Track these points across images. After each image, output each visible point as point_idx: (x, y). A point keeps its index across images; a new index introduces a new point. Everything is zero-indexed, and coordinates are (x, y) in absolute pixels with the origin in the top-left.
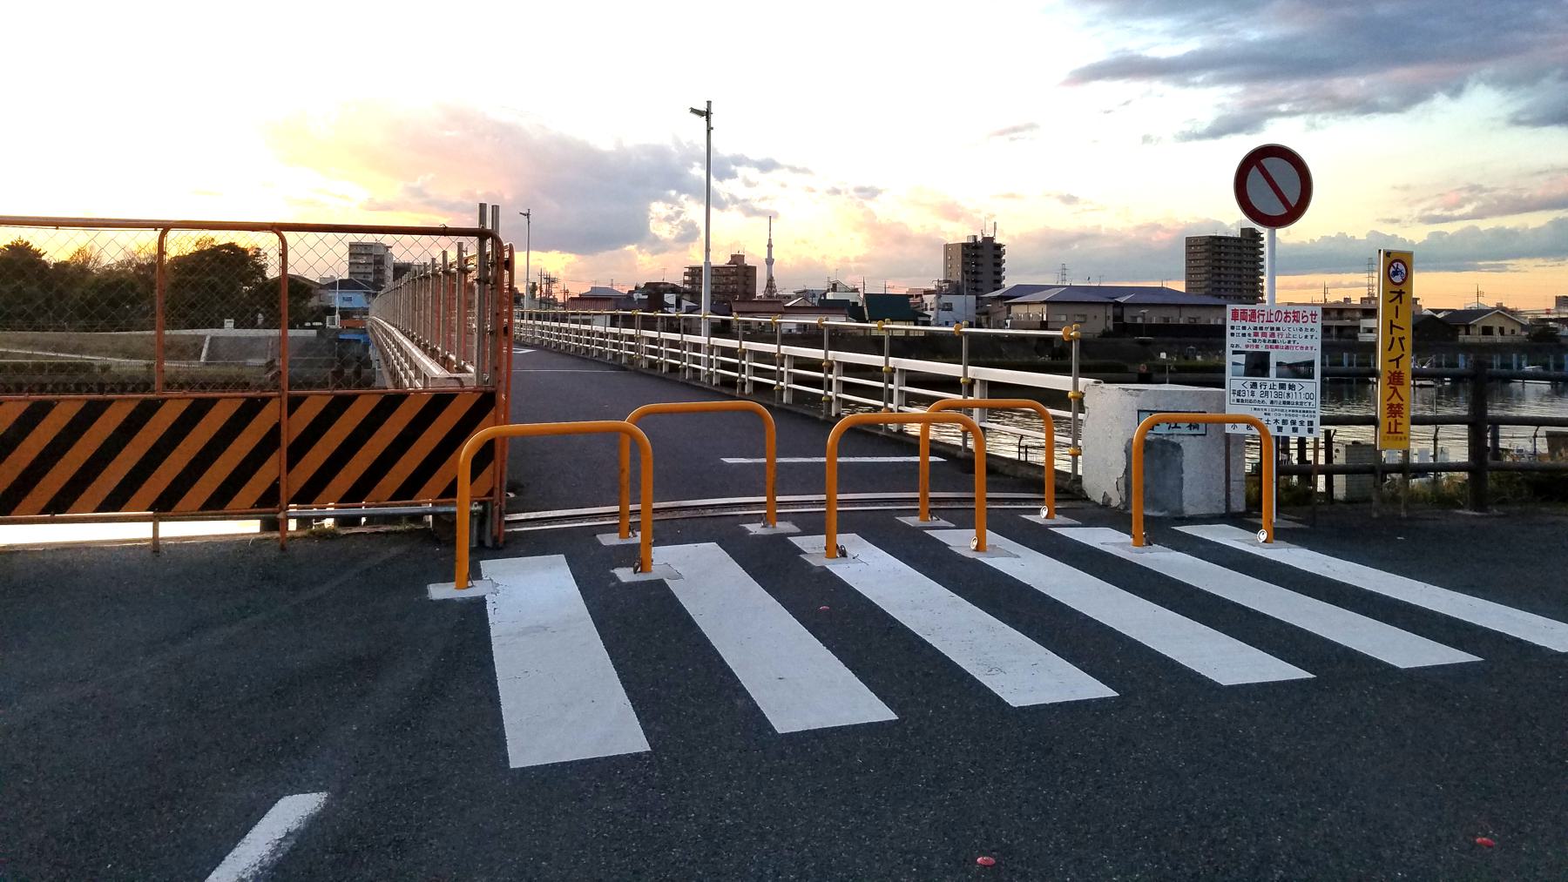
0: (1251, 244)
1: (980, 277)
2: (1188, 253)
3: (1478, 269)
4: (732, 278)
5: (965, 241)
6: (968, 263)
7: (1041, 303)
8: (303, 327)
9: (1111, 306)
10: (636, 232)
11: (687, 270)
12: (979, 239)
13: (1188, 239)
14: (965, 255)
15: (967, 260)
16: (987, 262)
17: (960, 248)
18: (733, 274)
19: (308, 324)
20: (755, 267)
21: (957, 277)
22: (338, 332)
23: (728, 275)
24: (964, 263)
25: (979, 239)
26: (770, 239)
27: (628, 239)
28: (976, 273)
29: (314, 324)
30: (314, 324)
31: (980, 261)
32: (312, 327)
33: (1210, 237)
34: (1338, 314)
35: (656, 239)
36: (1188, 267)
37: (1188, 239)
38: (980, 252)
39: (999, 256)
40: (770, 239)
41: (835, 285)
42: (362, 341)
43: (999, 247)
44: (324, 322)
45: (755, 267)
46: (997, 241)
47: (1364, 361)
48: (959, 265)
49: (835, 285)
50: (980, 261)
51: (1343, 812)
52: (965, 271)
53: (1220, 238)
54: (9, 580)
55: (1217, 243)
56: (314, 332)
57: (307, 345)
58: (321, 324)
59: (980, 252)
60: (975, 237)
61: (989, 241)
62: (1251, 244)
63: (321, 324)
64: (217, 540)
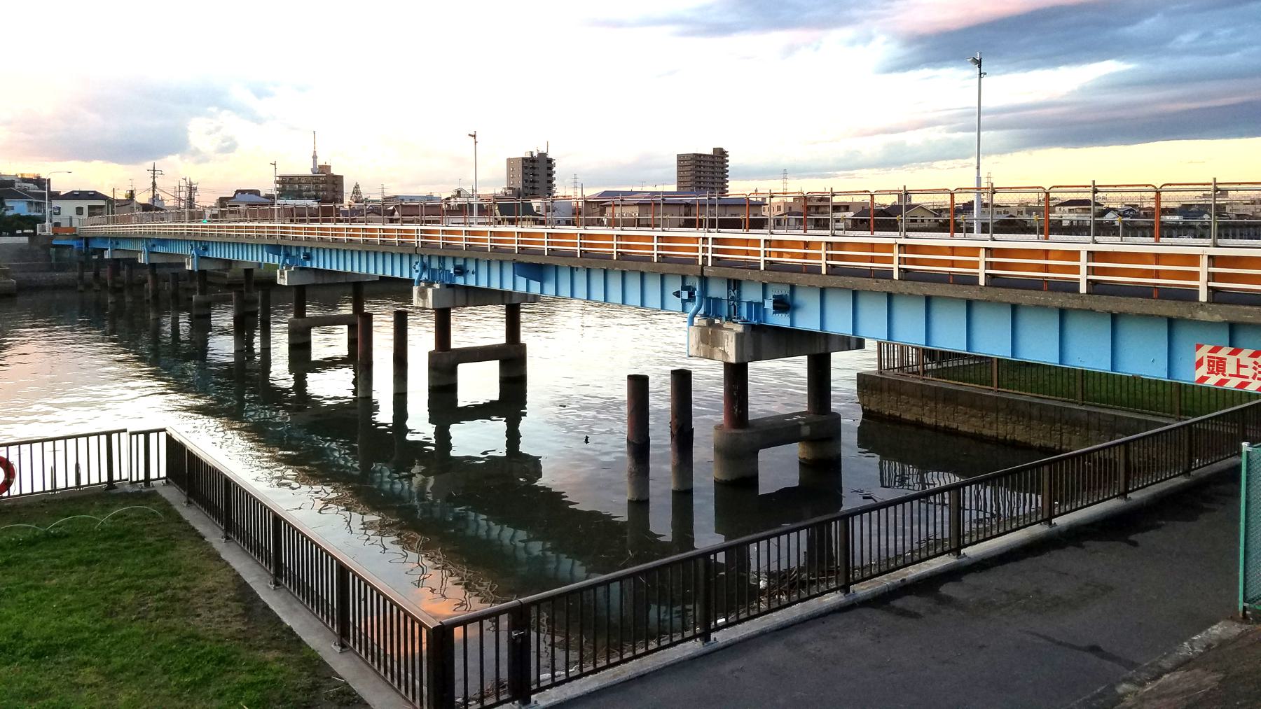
0: (720, 160)
1: (536, 185)
2: (679, 166)
3: (836, 176)
4: (321, 186)
5: (524, 156)
6: (526, 174)
7: (635, 205)
8: (13, 234)
9: (683, 206)
10: (174, 144)
11: (278, 179)
12: (535, 154)
13: (679, 156)
14: (524, 167)
15: (526, 171)
16: (542, 172)
17: (521, 162)
18: (323, 182)
19: (19, 232)
20: (342, 176)
21: (519, 185)
22: (50, 238)
23: (317, 183)
24: (524, 174)
25: (535, 154)
26: (315, 152)
27: (172, 151)
28: (533, 181)
29: (26, 231)
30: (26, 231)
31: (536, 172)
32: (24, 235)
33: (694, 154)
34: (816, 210)
35: (196, 152)
36: (679, 177)
37: (679, 156)
38: (536, 165)
39: (550, 168)
40: (315, 152)
41: (459, 192)
42: (76, 247)
43: (550, 161)
44: (35, 229)
45: (342, 176)
46: (549, 156)
47: (119, 219)
48: (520, 175)
49: (459, 192)
50: (536, 172)
51: (128, 647)
52: (525, 181)
53: (700, 155)
54: (878, 636)
55: (698, 158)
56: (25, 240)
57: (21, 252)
58: (32, 231)
59: (536, 165)
60: (532, 153)
61: (543, 156)
62: (720, 160)
63: (32, 231)
64: (1004, 551)
